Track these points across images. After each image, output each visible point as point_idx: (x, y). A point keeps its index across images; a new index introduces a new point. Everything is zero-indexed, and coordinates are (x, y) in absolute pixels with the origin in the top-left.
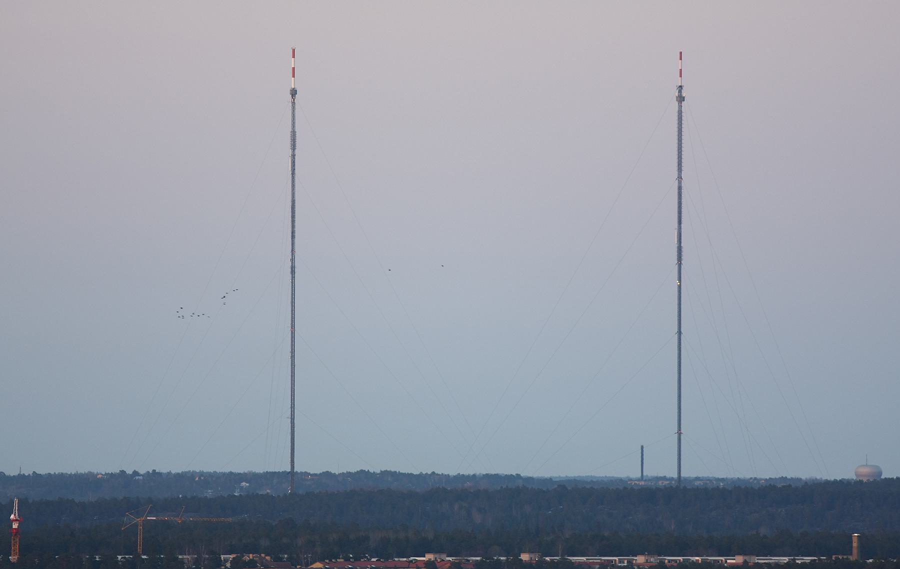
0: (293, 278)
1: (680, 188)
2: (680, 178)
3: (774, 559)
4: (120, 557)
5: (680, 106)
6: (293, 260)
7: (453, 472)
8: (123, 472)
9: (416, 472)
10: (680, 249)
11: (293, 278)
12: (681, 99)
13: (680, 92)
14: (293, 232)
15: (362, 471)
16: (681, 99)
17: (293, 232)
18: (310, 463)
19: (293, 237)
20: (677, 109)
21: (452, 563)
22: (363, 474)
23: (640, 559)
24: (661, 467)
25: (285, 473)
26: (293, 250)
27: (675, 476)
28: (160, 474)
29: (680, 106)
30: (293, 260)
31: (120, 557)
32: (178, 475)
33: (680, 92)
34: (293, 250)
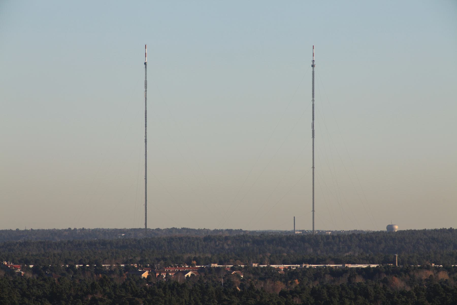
0: (146, 144)
1: (313, 105)
2: (313, 100)
3: (359, 266)
4: (77, 266)
5: (313, 69)
6: (146, 136)
7: (212, 228)
8: (70, 229)
9: (197, 228)
10: (146, 111)
11: (146, 144)
12: (313, 66)
13: (313, 63)
14: (146, 124)
15: (174, 228)
16: (313, 66)
17: (146, 124)
18: (152, 226)
19: (146, 126)
20: (312, 70)
21: (285, 269)
22: (188, 230)
23: (372, 266)
24: (304, 225)
25: (144, 229)
26: (146, 133)
27: (312, 230)
28: (85, 229)
29: (313, 69)
30: (146, 136)
31: (77, 266)
32: (93, 230)
33: (313, 63)
34: (146, 133)
